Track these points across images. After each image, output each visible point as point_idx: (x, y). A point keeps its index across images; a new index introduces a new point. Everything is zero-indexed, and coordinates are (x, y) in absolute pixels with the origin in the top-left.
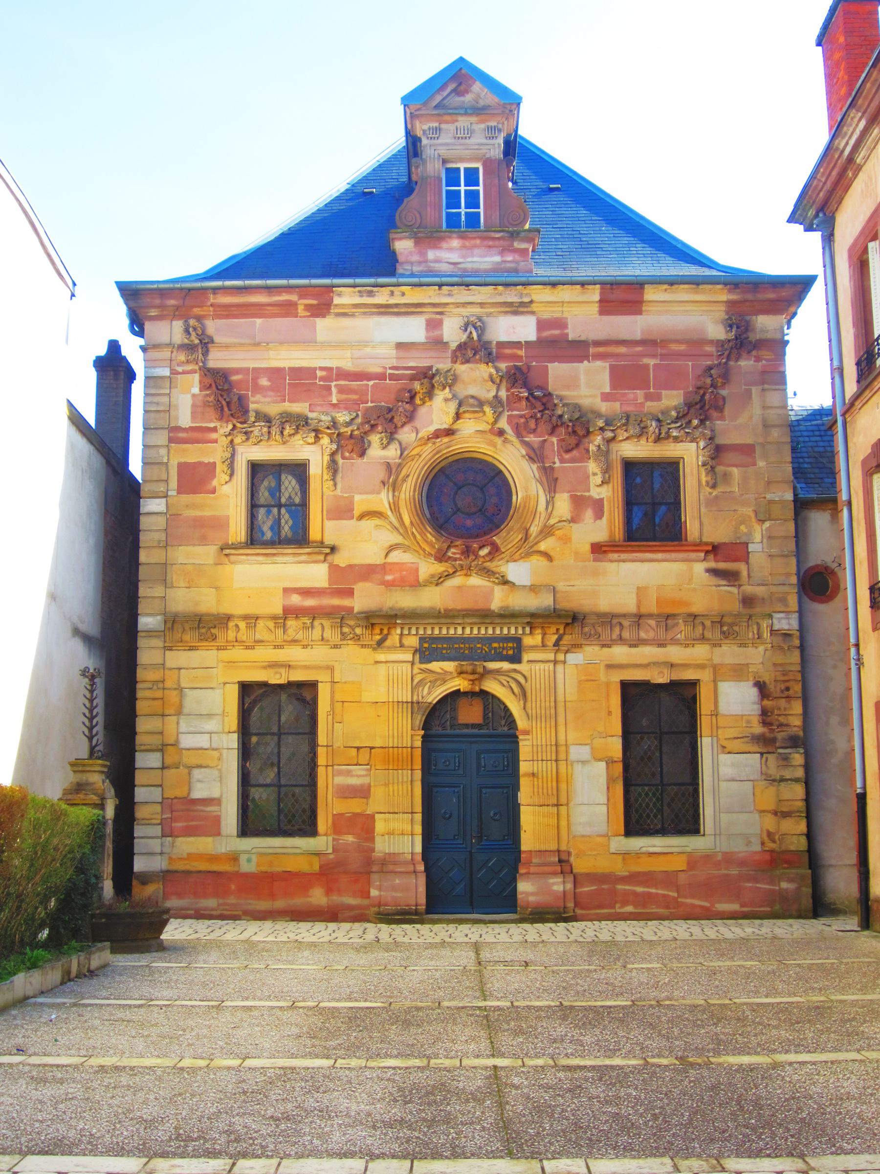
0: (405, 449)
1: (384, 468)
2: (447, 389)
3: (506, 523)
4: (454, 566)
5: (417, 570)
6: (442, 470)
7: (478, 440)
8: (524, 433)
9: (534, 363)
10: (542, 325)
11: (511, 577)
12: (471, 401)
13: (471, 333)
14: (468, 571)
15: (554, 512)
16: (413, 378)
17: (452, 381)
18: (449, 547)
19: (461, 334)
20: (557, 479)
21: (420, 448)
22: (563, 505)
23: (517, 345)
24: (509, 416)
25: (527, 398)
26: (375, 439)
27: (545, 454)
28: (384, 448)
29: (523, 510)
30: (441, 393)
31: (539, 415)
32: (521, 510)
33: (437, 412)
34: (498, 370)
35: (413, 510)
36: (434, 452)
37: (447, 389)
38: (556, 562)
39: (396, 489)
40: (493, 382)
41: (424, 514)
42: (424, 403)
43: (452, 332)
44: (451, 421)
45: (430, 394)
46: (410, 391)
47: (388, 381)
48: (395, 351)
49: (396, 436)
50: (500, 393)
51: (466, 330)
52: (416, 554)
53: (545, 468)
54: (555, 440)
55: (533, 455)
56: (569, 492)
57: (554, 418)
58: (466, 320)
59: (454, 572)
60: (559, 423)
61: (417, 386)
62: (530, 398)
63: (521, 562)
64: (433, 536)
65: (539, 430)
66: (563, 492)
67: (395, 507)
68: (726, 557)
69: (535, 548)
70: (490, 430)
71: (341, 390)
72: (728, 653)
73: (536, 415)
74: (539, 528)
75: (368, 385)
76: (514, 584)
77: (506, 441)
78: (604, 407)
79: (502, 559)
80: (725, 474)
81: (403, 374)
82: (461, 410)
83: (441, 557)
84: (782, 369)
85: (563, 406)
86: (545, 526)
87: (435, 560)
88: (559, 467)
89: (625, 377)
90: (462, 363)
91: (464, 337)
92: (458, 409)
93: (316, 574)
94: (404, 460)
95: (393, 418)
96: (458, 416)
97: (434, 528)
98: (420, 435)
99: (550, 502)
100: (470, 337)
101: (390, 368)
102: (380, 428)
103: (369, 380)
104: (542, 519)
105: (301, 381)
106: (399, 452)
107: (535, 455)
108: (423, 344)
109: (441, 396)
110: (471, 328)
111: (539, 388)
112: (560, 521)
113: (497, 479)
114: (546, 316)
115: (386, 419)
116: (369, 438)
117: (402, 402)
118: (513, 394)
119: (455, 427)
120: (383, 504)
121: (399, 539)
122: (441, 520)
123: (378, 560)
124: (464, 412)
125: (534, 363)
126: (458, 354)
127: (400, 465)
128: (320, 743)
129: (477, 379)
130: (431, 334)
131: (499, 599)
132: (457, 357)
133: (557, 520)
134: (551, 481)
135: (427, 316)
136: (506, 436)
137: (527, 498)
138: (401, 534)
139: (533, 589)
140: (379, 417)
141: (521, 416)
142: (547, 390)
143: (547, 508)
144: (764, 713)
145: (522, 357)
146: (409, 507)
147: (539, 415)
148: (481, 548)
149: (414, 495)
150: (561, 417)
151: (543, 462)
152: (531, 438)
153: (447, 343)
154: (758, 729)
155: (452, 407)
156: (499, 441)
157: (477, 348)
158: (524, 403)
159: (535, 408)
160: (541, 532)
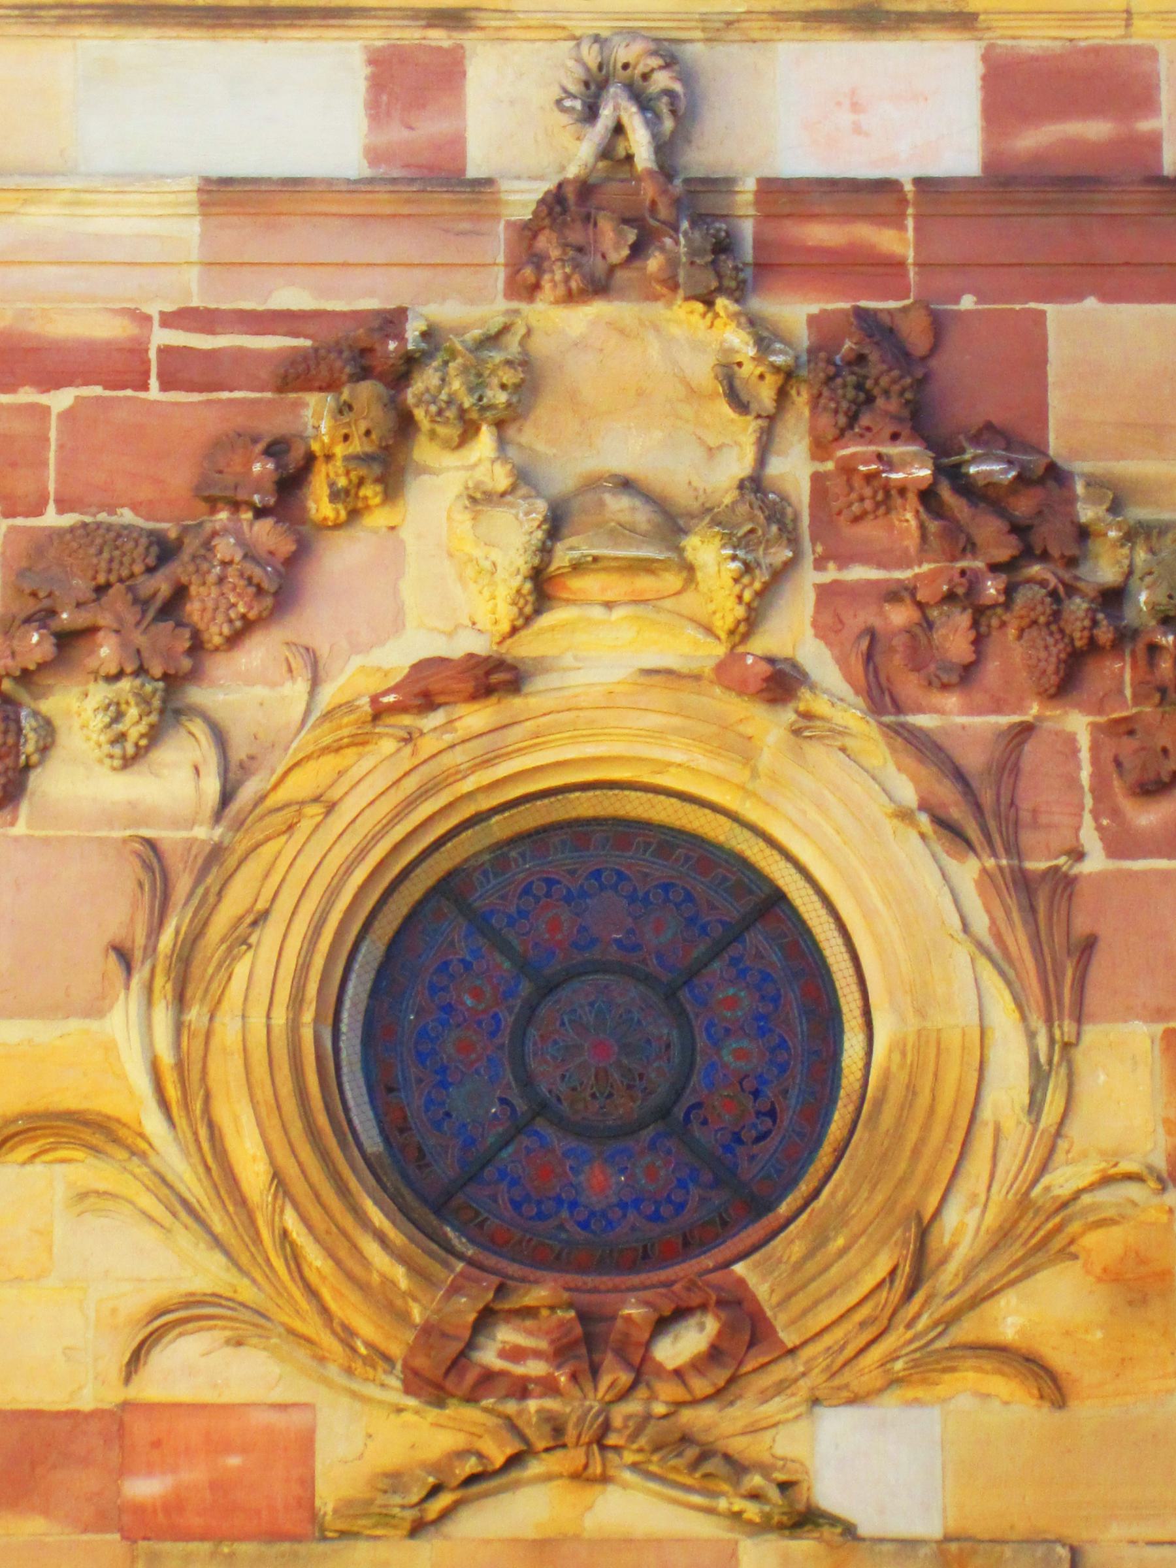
0: (246, 769)
1: (132, 870)
2: (486, 439)
3: (804, 1188)
4: (512, 1426)
5: (306, 1444)
6: (451, 888)
7: (655, 720)
8: (909, 686)
9: (968, 302)
10: (1013, 89)
11: (828, 1494)
12: (619, 505)
13: (619, 129)
14: (595, 1451)
15: (1074, 1129)
16: (296, 376)
17: (512, 393)
18: (486, 1319)
19: (566, 138)
20: (1088, 947)
21: (330, 763)
23: (874, 196)
24: (827, 594)
25: (927, 496)
26: (78, 711)
27: (1025, 806)
28: (128, 762)
29: (901, 1122)
30: (450, 460)
31: (992, 589)
32: (887, 1118)
33: (429, 563)
34: (765, 337)
35: (290, 1106)
36: (410, 785)
37: (486, 439)
38: (1085, 1411)
39: (194, 990)
40: (740, 404)
41: (346, 1132)
42: (354, 514)
43: (517, 126)
44: (506, 614)
45: (387, 465)
46: (276, 449)
47: (154, 392)
48: (193, 228)
49: (197, 695)
50: (777, 467)
51: (591, 113)
52: (302, 1354)
53: (1023, 884)
54: (1078, 724)
55: (958, 812)
56: (1159, 1014)
57: (1078, 607)
58: (591, 56)
59: (514, 1461)
60: (1104, 634)
61: (316, 417)
62: (946, 493)
63: (890, 1406)
64: (400, 1257)
65: (992, 668)
66: (1128, 1014)
67: (184, 1089)
69: (967, 1330)
70: (721, 668)
73: (973, 582)
74: (990, 1219)
75: (46, 411)
76: (849, 1530)
77: (806, 727)
79: (781, 1388)
80: (425, 335)
81: (240, 354)
82: (563, 556)
83: (443, 1373)
84: (311, 351)
85: (1130, 536)
86: (1024, 1203)
87: (408, 1390)
88: (1101, 879)
90: (570, 298)
91: (579, 154)
92: (545, 551)
94: (239, 825)
95: (180, 593)
96: (541, 589)
97: (402, 1211)
98: (328, 695)
99: (1054, 1069)
100: (613, 153)
101: (170, 320)
102: (106, 651)
103: (52, 381)
104: (1008, 1161)
106: (212, 786)
107: (974, 808)
108: (354, 187)
109: (449, 473)
110: (617, 106)
111: (991, 436)
112: (1106, 1180)
113: (756, 938)
114: (1038, 40)
115: (143, 603)
116: (47, 706)
117: (236, 506)
118: (847, 469)
119: (525, 648)
120: (123, 1077)
121: (206, 1272)
122: (446, 1168)
123: (92, 1389)
124: (577, 567)
125: (968, 302)
126: (547, 243)
127: (216, 853)
128: (502, 269)
129: (656, 385)
130: (396, 134)
132: (539, 262)
133: (1087, 1172)
135: (376, 35)
136: (806, 700)
137: (924, 1050)
138: (217, 1242)
140: (101, 590)
141: (894, 594)
142: (1040, 449)
143: (1035, 1107)
145: (899, 265)
146: (264, 1093)
147: (992, 589)
148: (663, 1324)
149: (294, 1026)
150: (1113, 598)
151: (1014, 849)
152: (945, 716)
153: (489, 182)
155: (513, 536)
156: (769, 726)
157: (646, 213)
158: (908, 517)
159: (971, 547)
160: (1003, 1235)
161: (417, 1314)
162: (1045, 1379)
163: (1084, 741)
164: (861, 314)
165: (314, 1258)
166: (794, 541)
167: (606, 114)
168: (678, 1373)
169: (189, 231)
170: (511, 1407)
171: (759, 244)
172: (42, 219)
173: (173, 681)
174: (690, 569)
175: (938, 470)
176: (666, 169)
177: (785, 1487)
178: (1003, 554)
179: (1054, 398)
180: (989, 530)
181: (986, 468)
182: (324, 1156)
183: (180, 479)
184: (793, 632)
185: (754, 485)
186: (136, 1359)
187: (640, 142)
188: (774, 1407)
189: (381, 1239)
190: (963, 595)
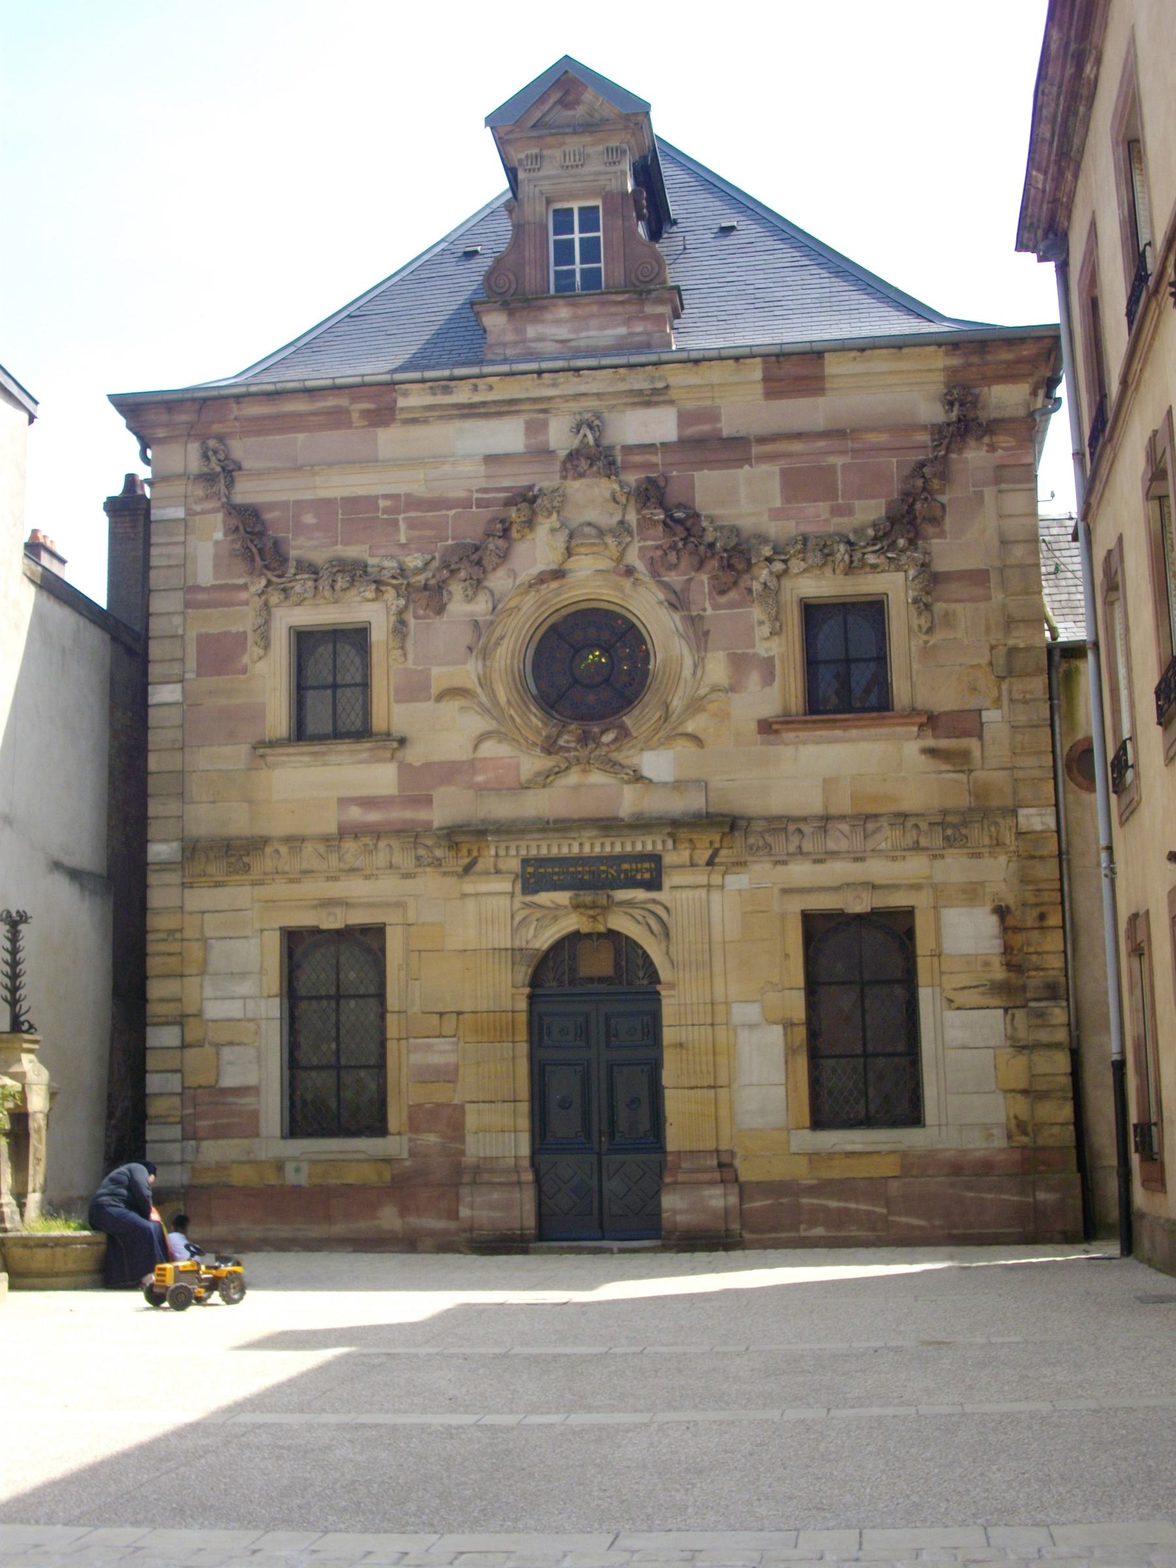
0: (499, 601)
2: (555, 516)
6: (553, 628)
8: (662, 571)
9: (675, 473)
10: (684, 419)
11: (646, 772)
12: (587, 530)
14: (586, 764)
16: (508, 503)
18: (559, 735)
20: (707, 633)
22: (717, 669)
23: (649, 448)
24: (641, 548)
25: (664, 522)
26: (456, 589)
30: (547, 521)
33: (539, 549)
37: (555, 516)
41: (527, 689)
43: (560, 435)
45: (530, 524)
46: (502, 521)
47: (474, 509)
48: (483, 468)
49: (486, 583)
51: (579, 431)
56: (725, 650)
57: (702, 548)
58: (578, 417)
61: (513, 513)
67: (485, 681)
68: (950, 730)
69: (680, 730)
71: (412, 525)
72: (954, 868)
76: (651, 781)
77: (637, 583)
78: (775, 529)
79: (634, 746)
83: (550, 747)
85: (715, 529)
89: (797, 484)
90: (574, 479)
91: (576, 443)
92: (569, 542)
93: (377, 776)
96: (569, 552)
101: (477, 491)
102: (462, 574)
105: (358, 513)
106: (490, 606)
107: (677, 601)
109: (544, 526)
110: (585, 430)
111: (680, 506)
121: (492, 725)
123: (465, 755)
125: (675, 473)
127: (492, 623)
131: (630, 802)
134: (699, 634)
135: (526, 417)
136: (636, 575)
139: (678, 785)
143: (694, 674)
144: (1007, 949)
148: (603, 733)
149: (512, 664)
150: (711, 545)
151: (689, 610)
154: (999, 973)
155: (561, 540)
156: (627, 583)
158: (661, 528)
159: (675, 534)
161: (544, 733)
162: (696, 739)
163: (706, 581)
164: (648, 478)
165: (518, 720)
166: (632, 536)
167: (582, 432)
168: (608, 745)
169: (482, 469)
170: (566, 755)
171: (622, 462)
172: (447, 468)
173: (479, 581)
174: (606, 544)
175: (666, 516)
176: (598, 445)
177: (634, 771)
178: (683, 536)
179: (697, 495)
180: (679, 529)
181: (679, 515)
182: (521, 697)
183: (480, 530)
184: (633, 557)
185: (622, 522)
186: (476, 747)
187: (590, 439)
188: (631, 752)
189: (535, 715)
190: (673, 547)
